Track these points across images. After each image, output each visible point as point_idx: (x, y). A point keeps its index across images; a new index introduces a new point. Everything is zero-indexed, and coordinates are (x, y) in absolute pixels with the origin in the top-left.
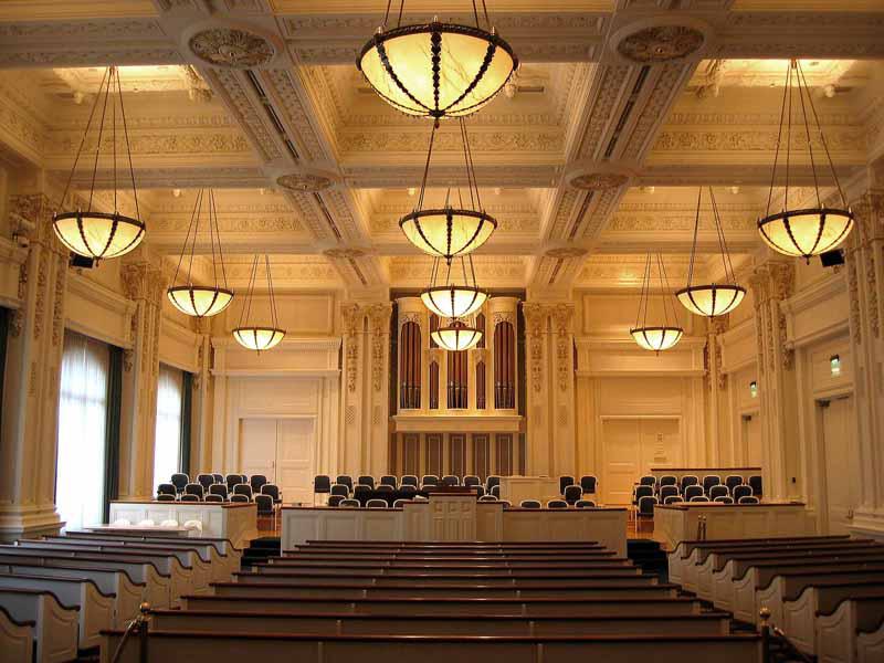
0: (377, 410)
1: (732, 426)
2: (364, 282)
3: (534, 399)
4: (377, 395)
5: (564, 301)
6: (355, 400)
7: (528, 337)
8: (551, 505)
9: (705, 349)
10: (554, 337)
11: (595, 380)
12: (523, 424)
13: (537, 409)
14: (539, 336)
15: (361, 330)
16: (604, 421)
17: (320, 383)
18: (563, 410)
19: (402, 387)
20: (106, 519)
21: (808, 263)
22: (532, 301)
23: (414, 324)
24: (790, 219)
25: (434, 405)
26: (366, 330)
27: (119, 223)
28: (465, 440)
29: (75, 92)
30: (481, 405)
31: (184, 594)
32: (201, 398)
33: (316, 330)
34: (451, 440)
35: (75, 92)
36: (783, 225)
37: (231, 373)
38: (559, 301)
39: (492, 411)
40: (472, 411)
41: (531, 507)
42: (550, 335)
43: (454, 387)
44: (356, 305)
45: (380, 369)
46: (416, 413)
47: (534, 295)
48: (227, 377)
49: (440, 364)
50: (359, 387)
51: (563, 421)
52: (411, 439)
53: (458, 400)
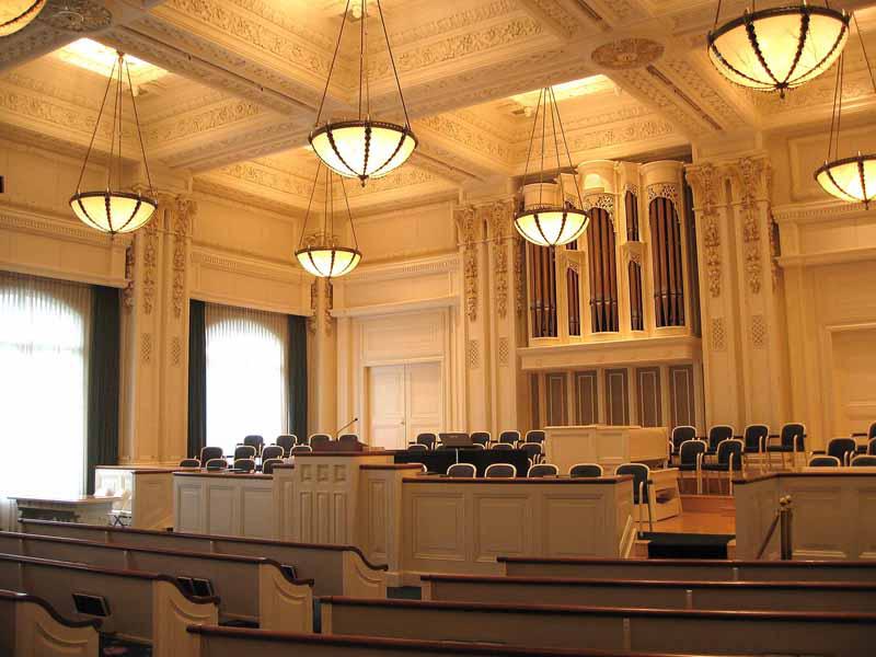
0: (503, 343)
2: (718, 127)
3: (714, 309)
4: (502, 323)
5: (752, 152)
6: (477, 332)
7: (698, 216)
8: (577, 471)
10: (491, 245)
11: (821, 271)
12: (697, 348)
13: (718, 324)
14: (713, 212)
15: (479, 241)
16: (835, 334)
17: (447, 313)
18: (757, 320)
19: (534, 309)
20: (778, 436)
21: (363, 185)
22: (703, 160)
23: (664, 200)
24: (757, 24)
25: (575, 330)
26: (729, 199)
27: (812, 17)
28: (691, 371)
30: (638, 324)
31: (501, 556)
32: (320, 344)
33: (425, 250)
34: (607, 376)
36: (364, 135)
37: (353, 312)
38: (739, 155)
39: (653, 332)
40: (625, 334)
41: (586, 474)
42: (729, 208)
43: (542, 307)
44: (472, 207)
45: (717, 263)
46: (549, 343)
47: (704, 152)
48: (351, 318)
49: (579, 272)
50: (480, 313)
51: (759, 338)
52: (556, 378)
53: (606, 320)
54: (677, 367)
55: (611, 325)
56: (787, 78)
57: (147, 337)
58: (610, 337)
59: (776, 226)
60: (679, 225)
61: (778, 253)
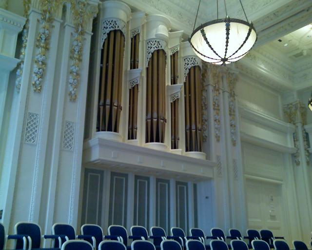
0: (67, 127)
1: (254, 177)
6: (41, 105)
9: (20, 36)
10: (68, 31)
16: (248, 180)
20: (46, 237)
25: (132, 136)
29: (303, 50)
35: (303, 50)
54: (93, 171)
55: (195, 148)
56: (225, 55)
57: (134, 65)
58: (154, 146)
59: (307, 134)
60: (102, 63)
61: (308, 145)
